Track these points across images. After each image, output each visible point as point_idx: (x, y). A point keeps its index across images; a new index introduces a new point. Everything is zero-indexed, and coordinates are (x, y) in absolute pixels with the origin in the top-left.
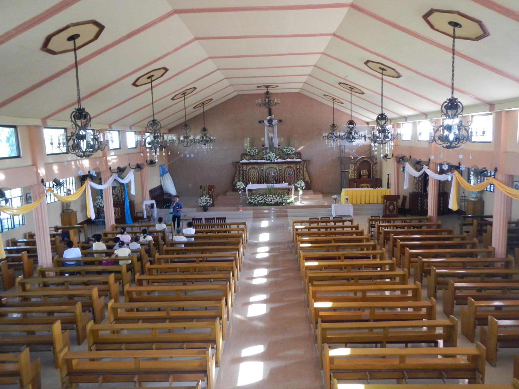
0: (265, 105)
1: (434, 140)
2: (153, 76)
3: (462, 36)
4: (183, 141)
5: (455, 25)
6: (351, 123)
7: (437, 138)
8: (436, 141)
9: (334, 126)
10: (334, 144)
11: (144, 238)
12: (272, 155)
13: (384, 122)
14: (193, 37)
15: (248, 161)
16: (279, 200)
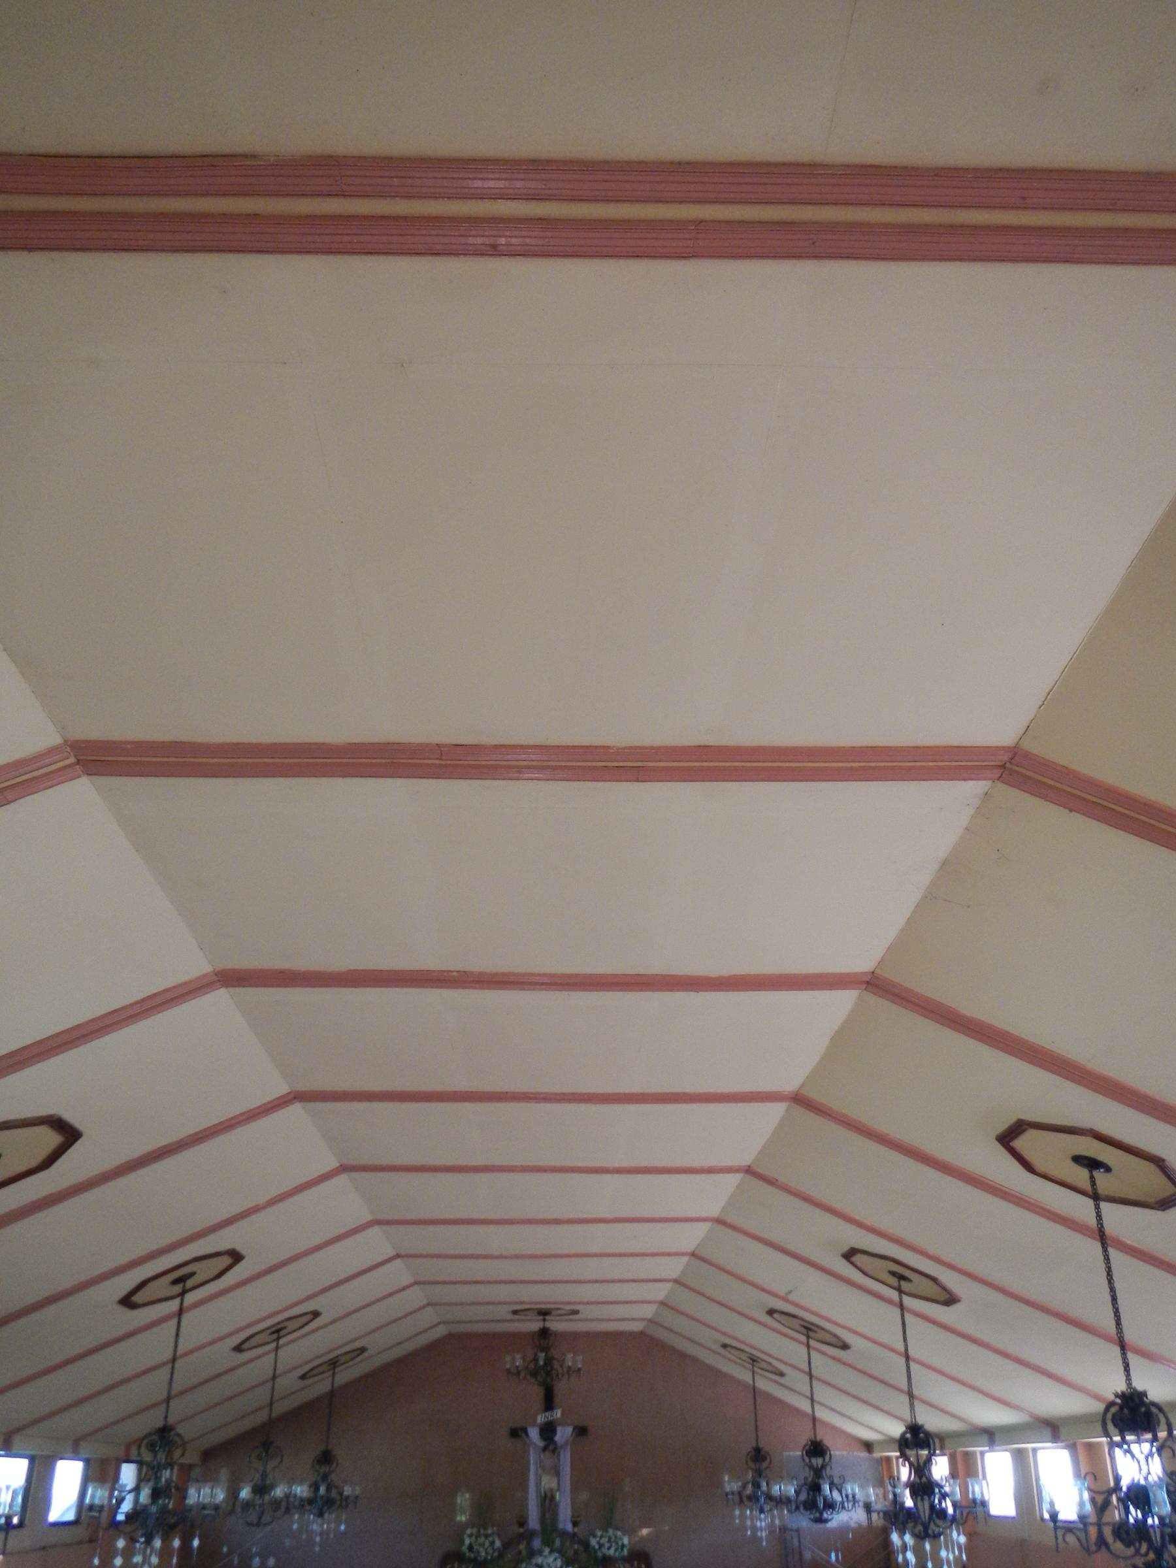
0: (534, 1374)
1: (1101, 1542)
2: (192, 1275)
3: (1117, 1195)
4: (247, 1505)
5: (1092, 1164)
6: (816, 1449)
7: (1109, 1537)
8: (1107, 1547)
9: (758, 1455)
10: (762, 1523)
13: (820, 1461)
14: (333, 1164)
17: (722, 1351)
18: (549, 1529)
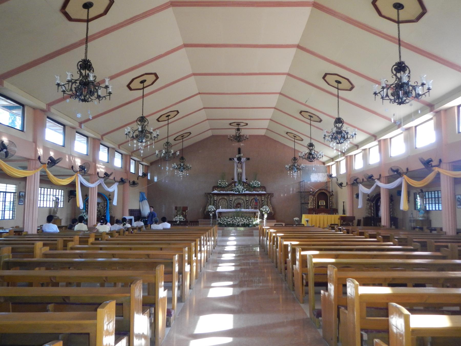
5: (339, 82)
8: (388, 97)
11: (124, 225)
12: (240, 187)
13: (340, 125)
15: (219, 192)
16: (245, 221)
17: (286, 136)
18: (240, 181)
